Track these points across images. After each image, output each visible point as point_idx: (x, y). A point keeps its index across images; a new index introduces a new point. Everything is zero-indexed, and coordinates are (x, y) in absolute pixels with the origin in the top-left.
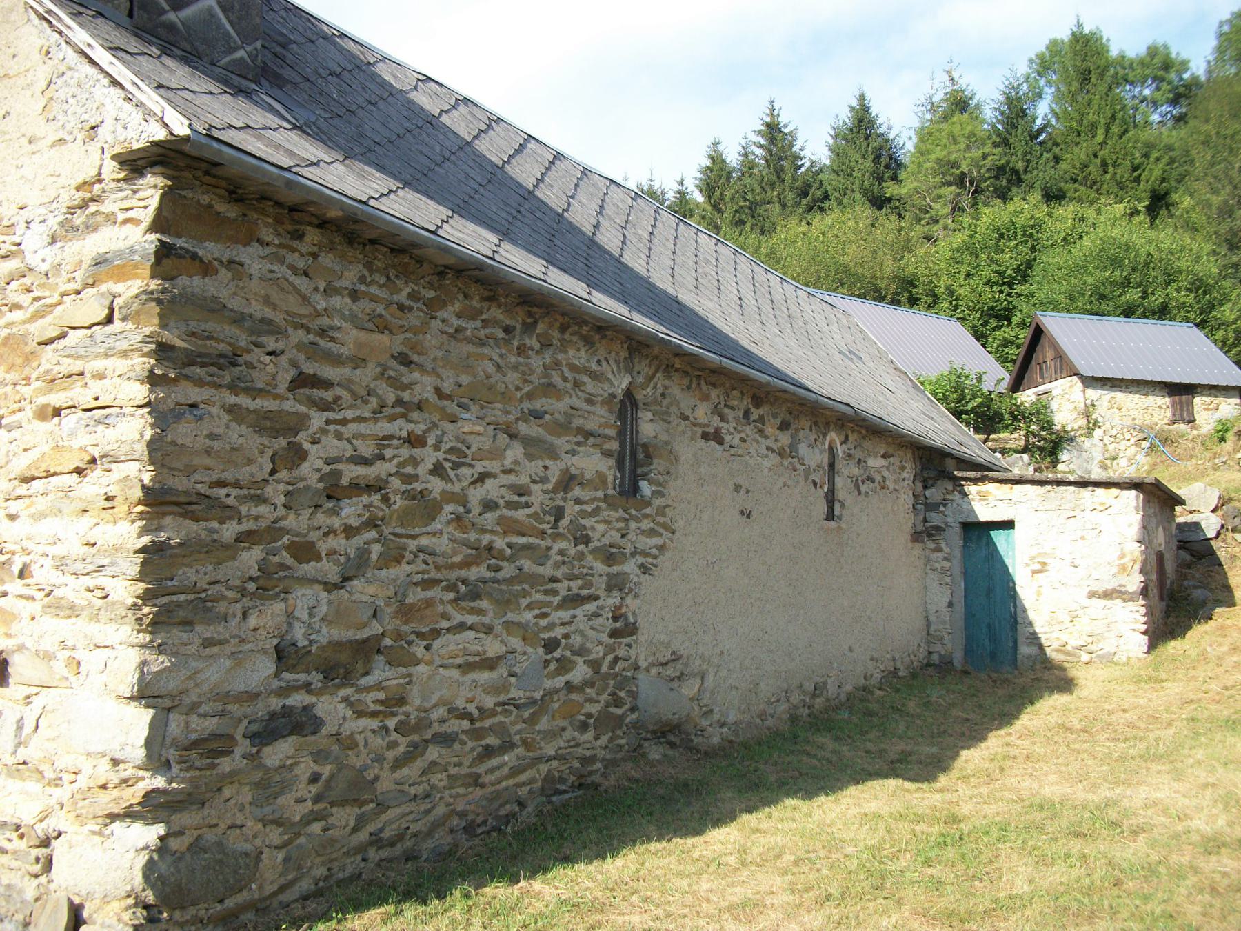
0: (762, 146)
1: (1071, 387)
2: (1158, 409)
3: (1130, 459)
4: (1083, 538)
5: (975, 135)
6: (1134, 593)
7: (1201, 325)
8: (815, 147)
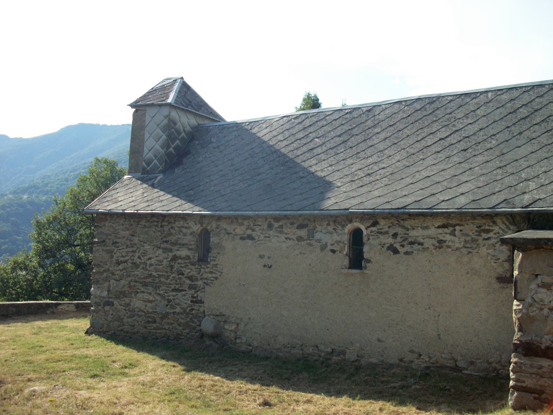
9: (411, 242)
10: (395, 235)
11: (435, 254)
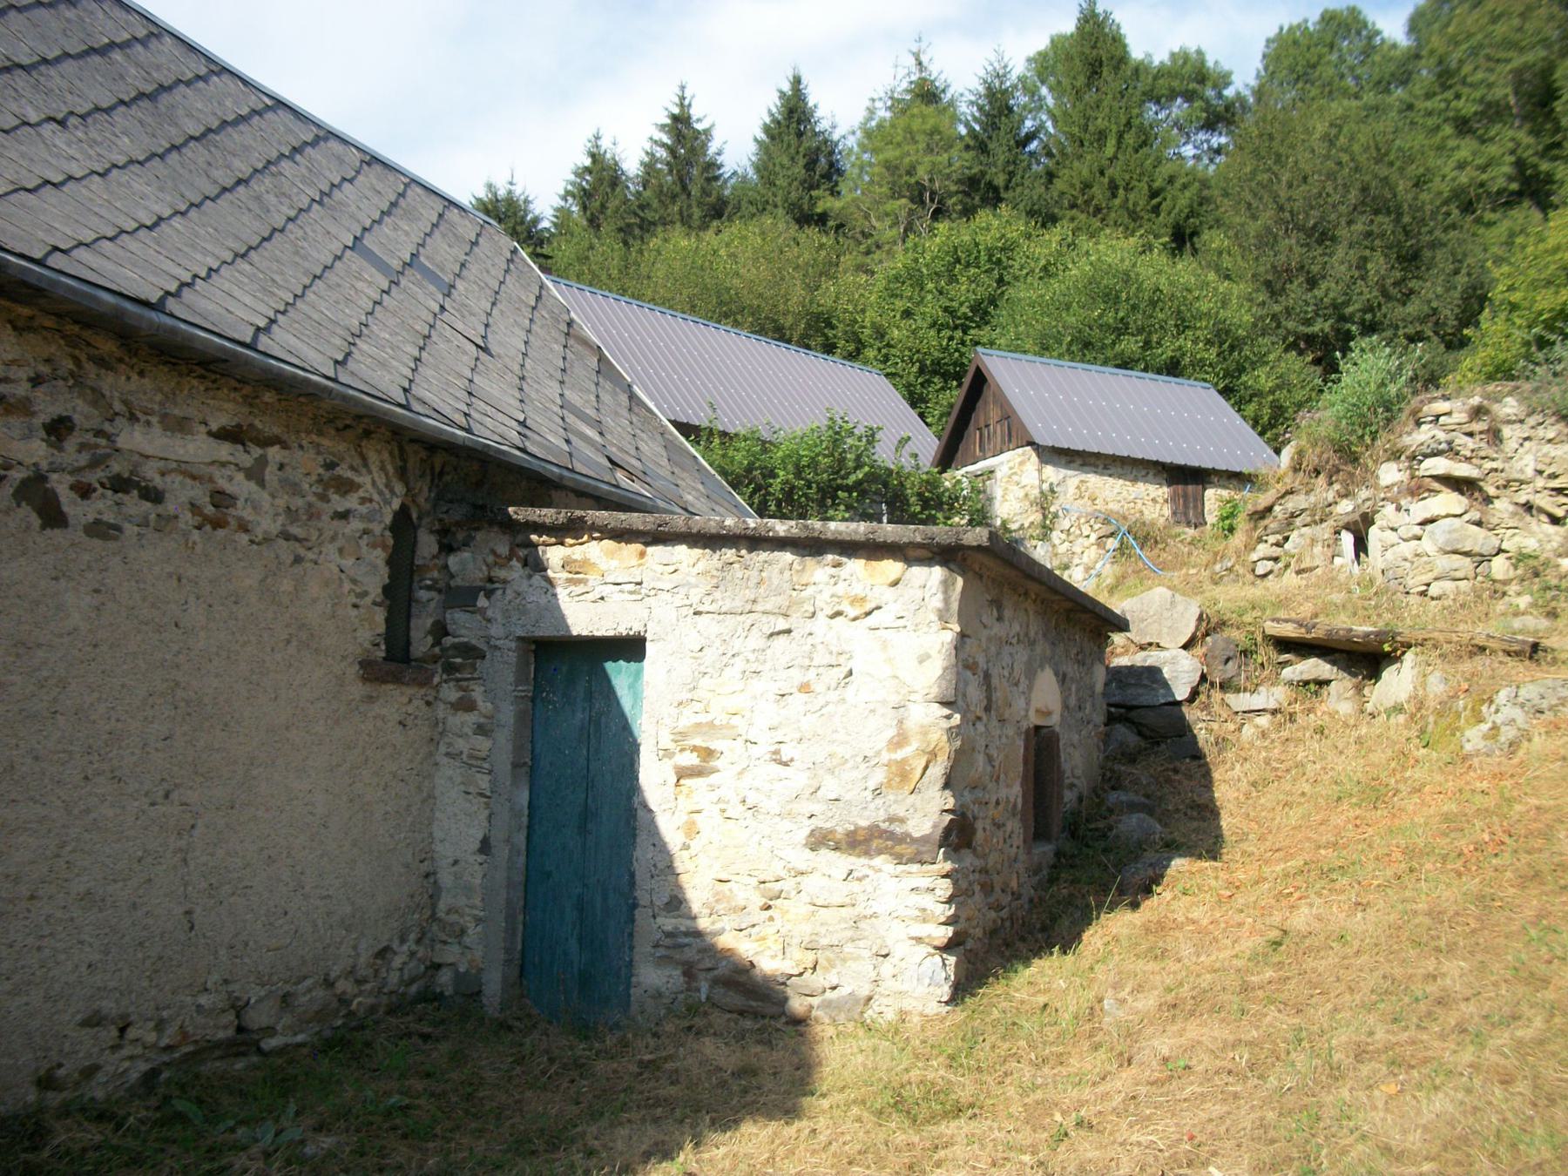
0: (663, 145)
1: (1022, 463)
2: (1150, 501)
3: (1088, 569)
4: (805, 688)
5: (940, 133)
6: (924, 840)
7: (1226, 392)
8: (736, 146)
9: (118, 477)
10: (58, 429)
11: (199, 548)
